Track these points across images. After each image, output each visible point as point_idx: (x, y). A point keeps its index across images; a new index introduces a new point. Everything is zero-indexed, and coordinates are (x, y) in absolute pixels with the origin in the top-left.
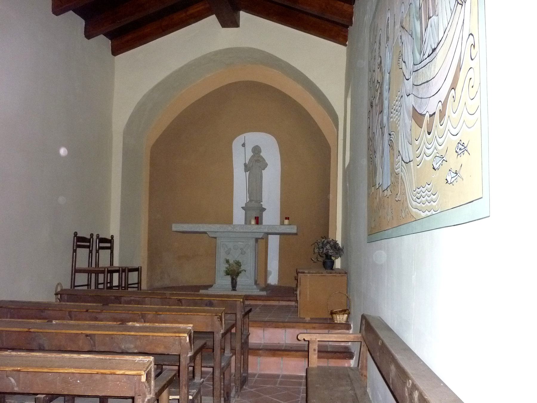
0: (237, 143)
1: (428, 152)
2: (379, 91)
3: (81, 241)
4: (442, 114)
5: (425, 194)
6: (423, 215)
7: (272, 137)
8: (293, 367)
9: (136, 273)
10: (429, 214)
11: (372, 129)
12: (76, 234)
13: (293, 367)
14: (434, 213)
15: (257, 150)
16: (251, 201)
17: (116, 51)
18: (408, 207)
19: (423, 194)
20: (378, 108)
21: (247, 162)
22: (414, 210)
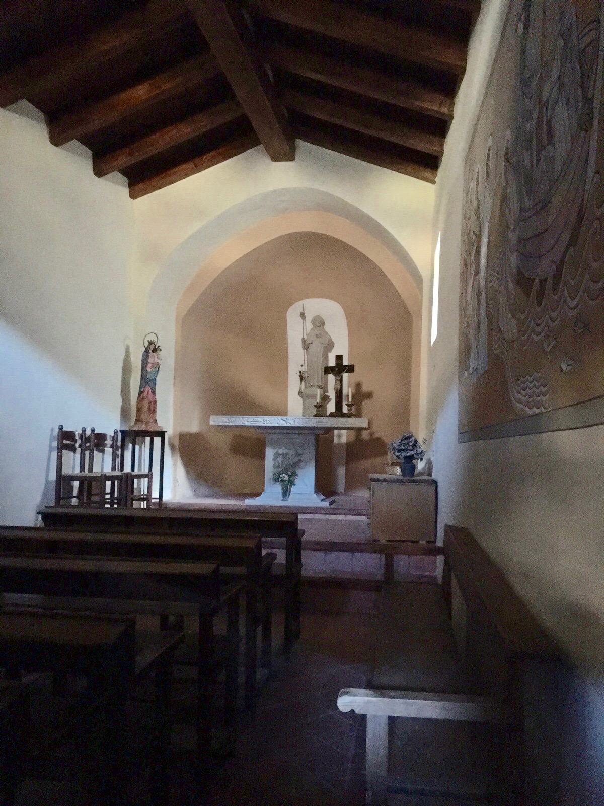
0: (292, 315)
1: (538, 329)
2: (475, 246)
3: (66, 440)
4: (557, 276)
5: (532, 384)
6: (530, 412)
7: (338, 304)
8: (108, 490)
9: (146, 479)
10: (537, 411)
11: (465, 296)
12: (61, 428)
13: (108, 490)
14: (545, 410)
15: (319, 323)
16: (356, 440)
17: (133, 196)
18: (510, 400)
19: (530, 386)
20: (473, 268)
21: (305, 337)
22: (518, 404)
